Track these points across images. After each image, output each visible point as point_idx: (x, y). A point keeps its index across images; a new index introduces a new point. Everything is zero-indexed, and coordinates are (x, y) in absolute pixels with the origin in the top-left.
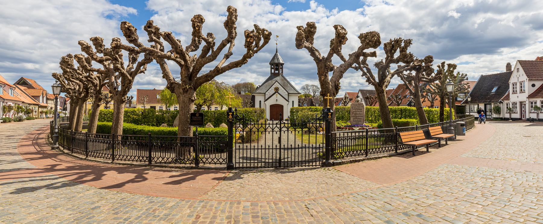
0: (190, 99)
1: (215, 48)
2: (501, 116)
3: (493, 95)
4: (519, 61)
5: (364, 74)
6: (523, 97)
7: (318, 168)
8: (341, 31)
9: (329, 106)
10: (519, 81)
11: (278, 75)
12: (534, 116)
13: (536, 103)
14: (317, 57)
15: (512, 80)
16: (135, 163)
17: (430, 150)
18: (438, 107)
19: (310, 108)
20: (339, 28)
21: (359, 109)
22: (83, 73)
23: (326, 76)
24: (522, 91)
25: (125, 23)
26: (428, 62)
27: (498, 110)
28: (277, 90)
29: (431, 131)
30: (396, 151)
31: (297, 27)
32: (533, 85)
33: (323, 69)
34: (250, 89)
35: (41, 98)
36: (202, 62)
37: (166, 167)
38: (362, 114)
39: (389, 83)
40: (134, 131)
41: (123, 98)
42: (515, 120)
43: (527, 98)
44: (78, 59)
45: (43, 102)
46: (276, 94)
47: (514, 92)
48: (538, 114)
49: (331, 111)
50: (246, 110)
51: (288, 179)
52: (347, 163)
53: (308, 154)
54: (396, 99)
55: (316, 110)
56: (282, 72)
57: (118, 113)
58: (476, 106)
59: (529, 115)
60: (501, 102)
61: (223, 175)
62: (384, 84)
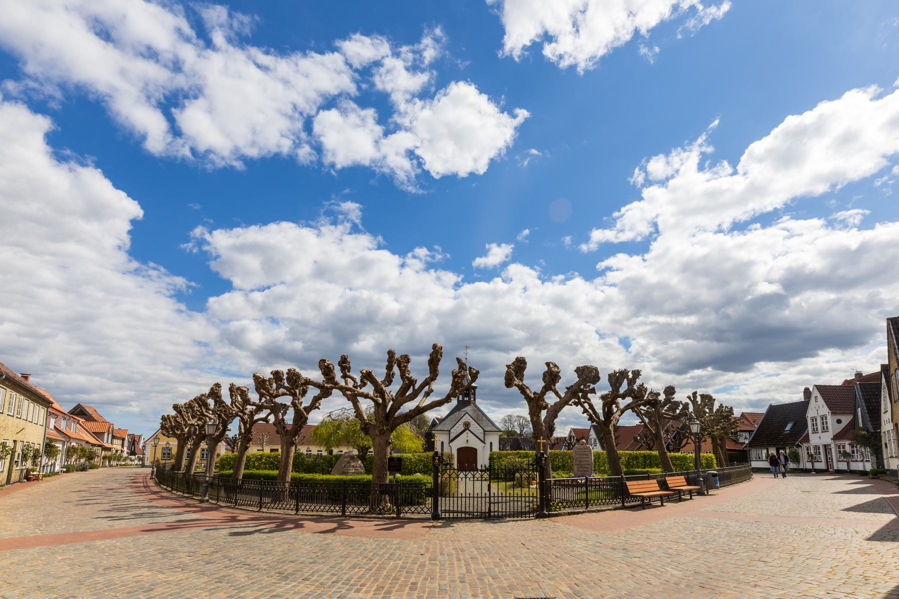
0: (387, 441)
1: (417, 386)
2: (801, 467)
3: (788, 434)
4: (816, 386)
5: (585, 411)
6: (826, 438)
7: (532, 519)
8: (553, 369)
9: (543, 450)
10: (819, 415)
11: (468, 403)
12: (843, 466)
13: (844, 447)
14: (528, 396)
15: (811, 413)
16: (324, 514)
17: (665, 504)
18: (692, 453)
19: (518, 453)
20: (551, 366)
21: (585, 455)
22: (233, 407)
23: (539, 417)
24: (825, 430)
25: (324, 361)
26: (669, 394)
27: (796, 458)
28: (467, 426)
29: (668, 482)
30: (623, 503)
31: (507, 366)
32: (839, 421)
33: (535, 408)
34: (419, 421)
35: (106, 435)
36: (402, 401)
37: (363, 517)
38: (589, 461)
39: (618, 421)
40: (301, 480)
41: (294, 439)
42: (819, 472)
43: (832, 439)
44: (241, 392)
45: (107, 442)
46: (466, 432)
47: (815, 431)
48: (848, 464)
49: (545, 456)
50: (427, 455)
51: (501, 527)
52: (565, 514)
53: (519, 506)
54: (646, 440)
55: (526, 456)
56: (475, 400)
57: (288, 457)
58: (764, 451)
59: (837, 466)
60: (798, 446)
61: (431, 524)
62: (610, 423)
